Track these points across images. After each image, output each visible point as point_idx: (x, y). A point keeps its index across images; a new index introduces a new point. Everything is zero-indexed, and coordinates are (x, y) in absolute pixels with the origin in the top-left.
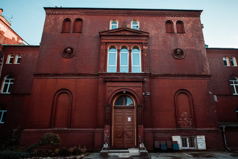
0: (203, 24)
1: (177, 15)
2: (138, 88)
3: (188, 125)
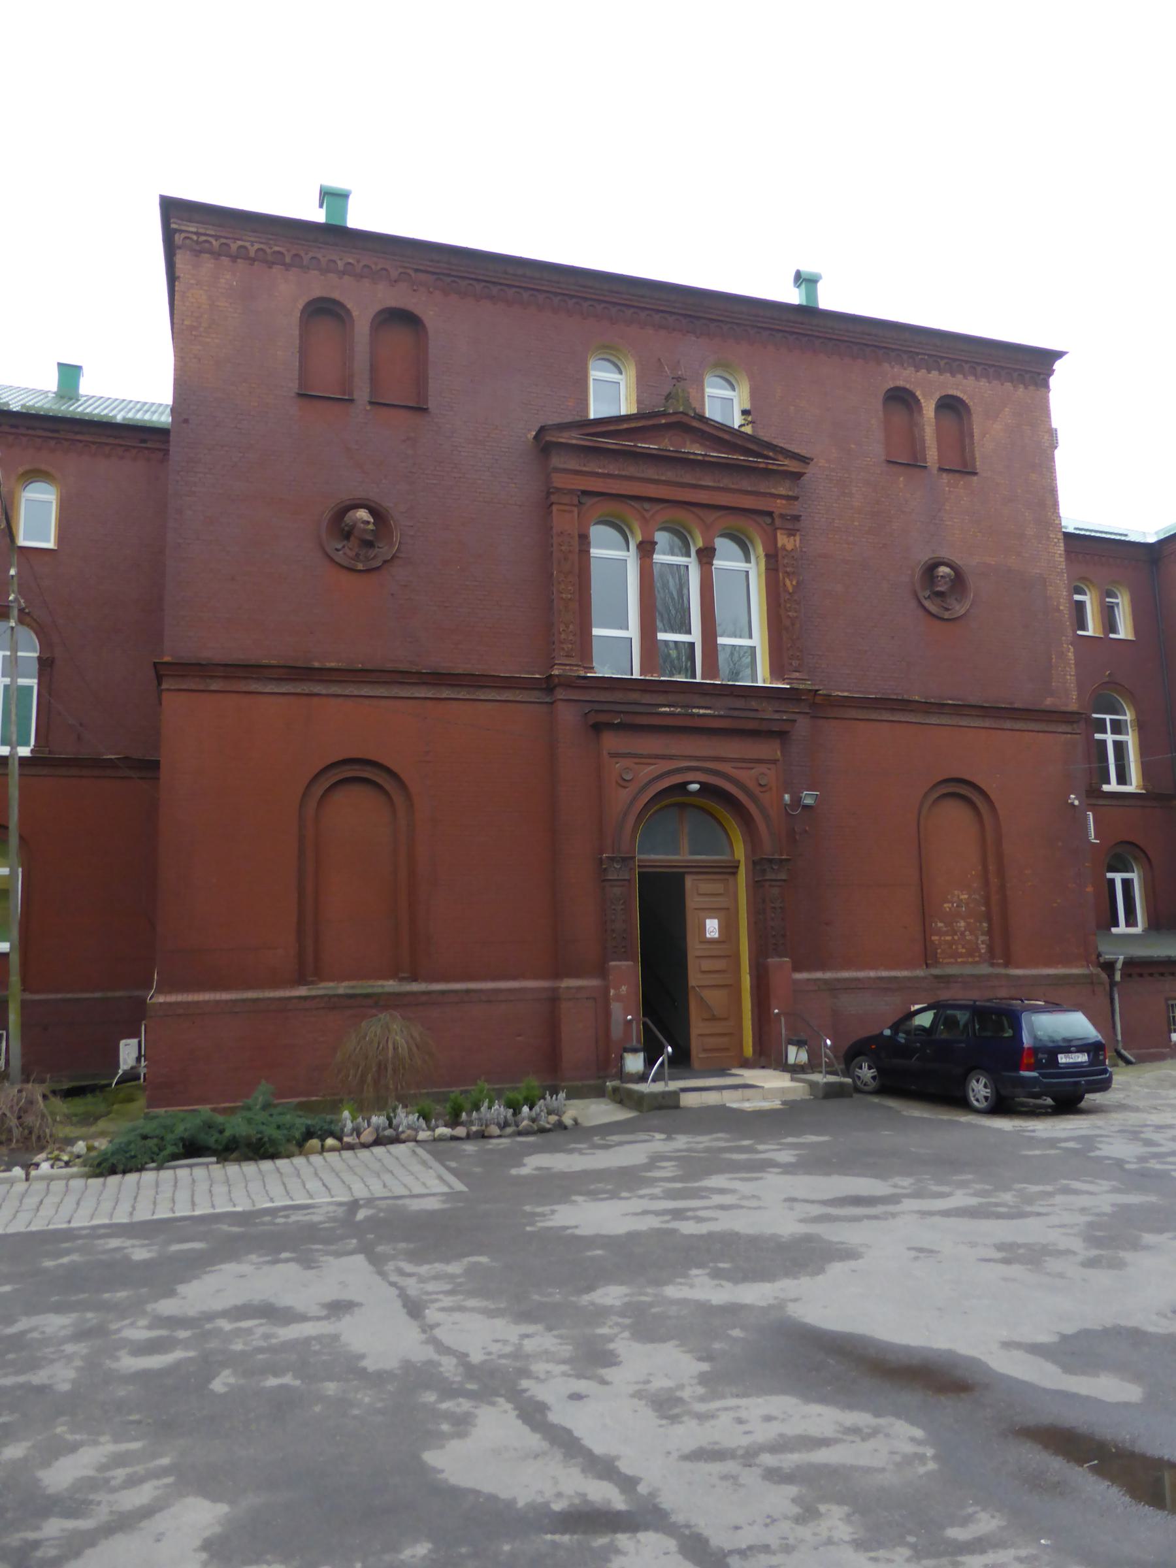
0: (1056, 430)
2: (762, 768)
3: (971, 954)
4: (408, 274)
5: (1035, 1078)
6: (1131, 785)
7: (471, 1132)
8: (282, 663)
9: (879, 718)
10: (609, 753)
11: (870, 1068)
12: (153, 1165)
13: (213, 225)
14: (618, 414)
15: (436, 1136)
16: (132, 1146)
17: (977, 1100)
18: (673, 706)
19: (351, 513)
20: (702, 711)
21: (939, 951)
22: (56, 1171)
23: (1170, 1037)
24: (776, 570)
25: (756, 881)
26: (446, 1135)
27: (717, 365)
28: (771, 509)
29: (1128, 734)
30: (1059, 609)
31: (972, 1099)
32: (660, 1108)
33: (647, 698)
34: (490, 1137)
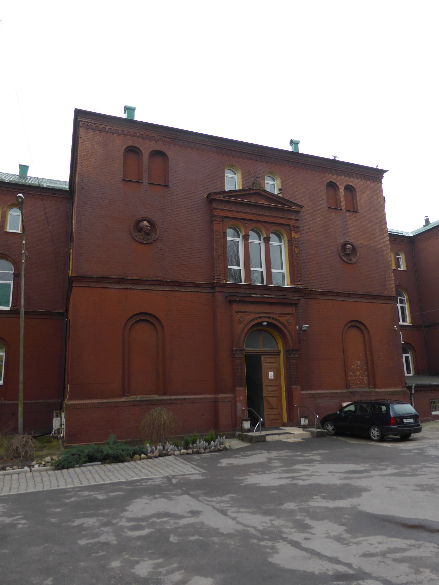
1: (346, 172)
2: (288, 317)
4: (162, 138)
5: (396, 428)
6: (407, 322)
7: (194, 451)
8: (117, 277)
9: (328, 299)
10: (235, 311)
11: (331, 426)
12: (78, 465)
13: (94, 119)
14: (234, 189)
15: (181, 453)
16: (69, 458)
17: (374, 437)
18: (257, 294)
19: (141, 223)
20: (267, 296)
21: (351, 383)
22: (40, 468)
23: (431, 413)
24: (292, 245)
25: (287, 358)
26: (185, 453)
27: (269, 173)
28: (289, 224)
29: (405, 304)
30: (388, 260)
31: (372, 436)
32: (258, 442)
33: (248, 291)
34: (201, 453)
